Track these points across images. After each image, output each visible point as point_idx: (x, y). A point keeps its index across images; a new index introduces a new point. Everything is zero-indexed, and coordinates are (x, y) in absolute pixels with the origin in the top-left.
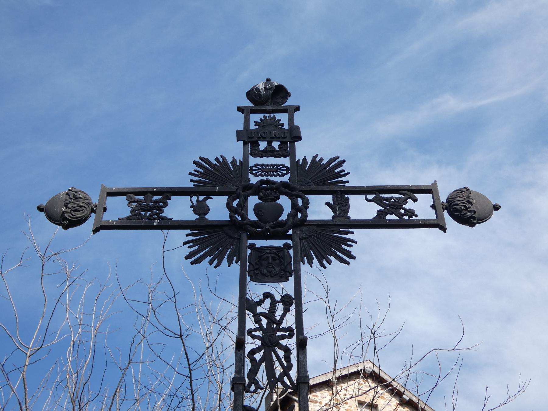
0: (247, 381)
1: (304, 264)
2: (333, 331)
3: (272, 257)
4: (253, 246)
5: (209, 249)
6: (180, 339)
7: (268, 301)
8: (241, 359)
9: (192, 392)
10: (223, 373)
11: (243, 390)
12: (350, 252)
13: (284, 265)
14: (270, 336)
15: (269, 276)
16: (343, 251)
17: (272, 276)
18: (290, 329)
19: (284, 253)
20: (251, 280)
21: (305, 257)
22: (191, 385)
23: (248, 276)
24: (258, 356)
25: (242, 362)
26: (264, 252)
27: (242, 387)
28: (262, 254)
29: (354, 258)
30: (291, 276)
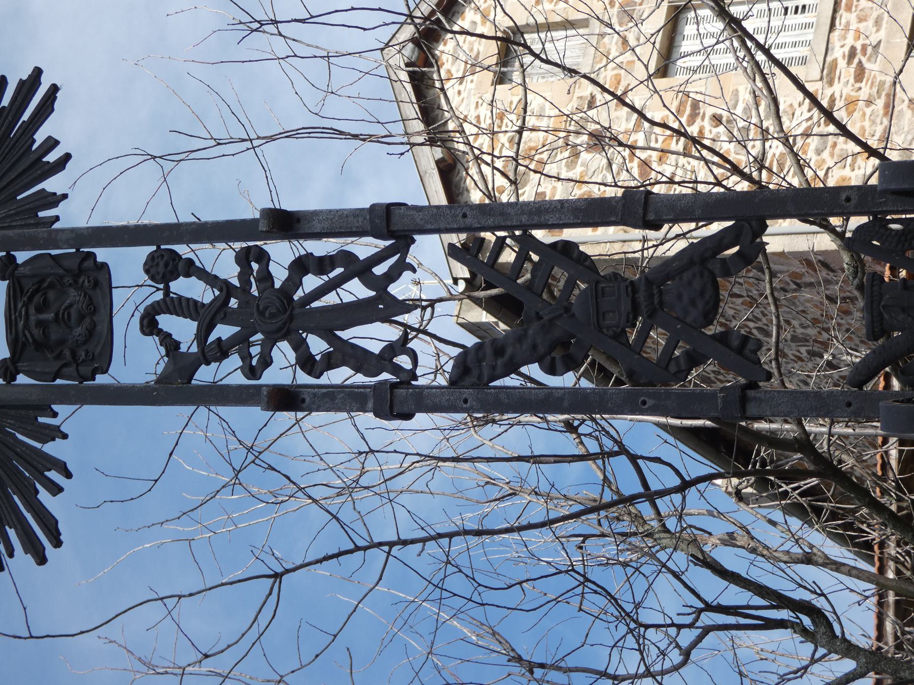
0: (385, 376)
1: (57, 218)
2: (256, 143)
3: (39, 310)
4: (7, 368)
5: (16, 498)
6: (284, 577)
7: (166, 322)
8: (325, 394)
9: (432, 538)
10: (377, 451)
11: (408, 389)
12: (22, 83)
13: (62, 277)
14: (261, 313)
15: (95, 318)
16: (17, 103)
17: (95, 312)
18: (243, 259)
19: (25, 276)
20: (105, 371)
21: (37, 216)
22: (413, 542)
23: (94, 380)
24: (317, 345)
25: (333, 392)
26: (25, 335)
27: (401, 392)
28: (31, 340)
29: (37, 73)
30: (93, 255)
